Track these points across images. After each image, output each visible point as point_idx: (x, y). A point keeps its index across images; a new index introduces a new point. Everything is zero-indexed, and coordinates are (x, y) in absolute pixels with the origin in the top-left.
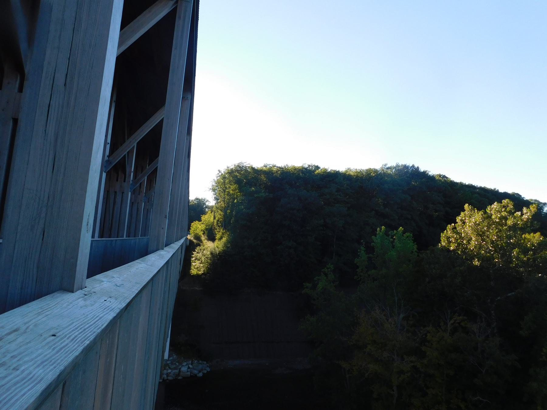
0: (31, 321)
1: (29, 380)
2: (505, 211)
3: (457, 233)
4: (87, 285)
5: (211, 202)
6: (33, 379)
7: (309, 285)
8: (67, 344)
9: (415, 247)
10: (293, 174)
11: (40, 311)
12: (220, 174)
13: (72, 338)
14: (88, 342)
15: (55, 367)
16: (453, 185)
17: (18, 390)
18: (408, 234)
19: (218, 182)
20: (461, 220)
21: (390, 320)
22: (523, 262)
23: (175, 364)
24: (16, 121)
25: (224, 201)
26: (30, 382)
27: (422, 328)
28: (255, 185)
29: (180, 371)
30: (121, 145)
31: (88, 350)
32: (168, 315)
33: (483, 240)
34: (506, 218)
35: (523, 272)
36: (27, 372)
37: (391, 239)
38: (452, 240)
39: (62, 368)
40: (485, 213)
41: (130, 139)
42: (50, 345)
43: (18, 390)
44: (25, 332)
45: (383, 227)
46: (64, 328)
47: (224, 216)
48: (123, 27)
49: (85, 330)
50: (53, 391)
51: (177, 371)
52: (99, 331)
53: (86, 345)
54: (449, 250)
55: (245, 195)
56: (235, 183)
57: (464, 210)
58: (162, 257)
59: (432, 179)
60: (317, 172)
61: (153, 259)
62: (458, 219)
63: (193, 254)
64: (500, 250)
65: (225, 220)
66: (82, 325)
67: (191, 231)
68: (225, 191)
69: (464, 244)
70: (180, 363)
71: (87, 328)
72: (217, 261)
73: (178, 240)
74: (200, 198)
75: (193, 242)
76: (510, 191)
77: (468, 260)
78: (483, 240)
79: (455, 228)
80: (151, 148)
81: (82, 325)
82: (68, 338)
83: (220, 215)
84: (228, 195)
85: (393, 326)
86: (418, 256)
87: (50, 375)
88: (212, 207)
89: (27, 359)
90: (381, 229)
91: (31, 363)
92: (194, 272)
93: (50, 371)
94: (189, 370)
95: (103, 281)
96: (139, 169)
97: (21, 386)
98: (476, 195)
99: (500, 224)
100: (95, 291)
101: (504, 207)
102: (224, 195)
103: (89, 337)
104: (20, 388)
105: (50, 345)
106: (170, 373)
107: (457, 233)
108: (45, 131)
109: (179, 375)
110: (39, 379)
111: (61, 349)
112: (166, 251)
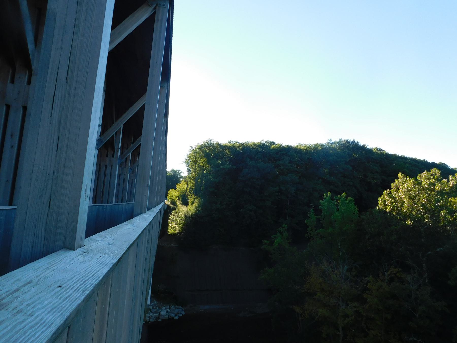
0: (41, 274)
1: (42, 324)
2: (433, 178)
3: (392, 197)
4: (85, 244)
5: (185, 173)
6: (45, 324)
7: (268, 242)
8: (71, 294)
9: (357, 209)
10: (253, 149)
11: (48, 266)
12: (192, 149)
13: (75, 288)
14: (88, 292)
15: (62, 314)
16: (388, 157)
17: (33, 333)
18: (350, 198)
19: (190, 156)
20: (396, 186)
21: (336, 271)
22: (449, 222)
23: (156, 309)
24: (25, 108)
25: (195, 172)
26: (42, 326)
27: (363, 278)
28: (221, 158)
29: (160, 315)
30: (110, 127)
31: (88, 299)
32: (150, 268)
33: (415, 203)
34: (434, 185)
35: (450, 231)
36: (40, 317)
37: (336, 203)
38: (388, 203)
39: (68, 314)
40: (416, 180)
41: (118, 122)
42: (57, 295)
43: (33, 333)
44: (37, 284)
45: (329, 193)
46: (68, 281)
47: (195, 184)
48: (113, 28)
49: (85, 282)
50: (61, 333)
51: (157, 314)
52: (97, 282)
53: (86, 294)
54: (385, 212)
55: (212, 167)
56: (204, 157)
57: (398, 178)
58: (145, 219)
59: (370, 151)
60: (273, 146)
61: (138, 221)
62: (393, 185)
63: (170, 216)
64: (430, 211)
65: (196, 188)
66: (82, 277)
67: (168, 197)
68: (196, 163)
69: (398, 207)
70: (160, 308)
71: (87, 280)
72: (191, 222)
73: (157, 205)
74: (176, 170)
75: (170, 207)
76: (437, 162)
77: (402, 220)
78: (415, 203)
79: (391, 193)
80: (134, 129)
81: (82, 277)
82: (72, 289)
83: (192, 184)
84: (198, 167)
85: (338, 276)
86: (359, 217)
87: (58, 320)
88: (186, 177)
89: (39, 306)
90: (327, 194)
91: (43, 310)
92: (171, 231)
93: (59, 317)
94: (167, 313)
95: (98, 240)
96: (125, 146)
97: (35, 330)
98: (407, 165)
99: (429, 189)
100: (92, 249)
101: (432, 175)
102: (196, 167)
103: (88, 288)
104: (35, 331)
105: (57, 295)
106: (152, 316)
107: (392, 197)
108: (51, 117)
109: (158, 318)
110: (50, 323)
111: (66, 298)
112: (148, 214)
